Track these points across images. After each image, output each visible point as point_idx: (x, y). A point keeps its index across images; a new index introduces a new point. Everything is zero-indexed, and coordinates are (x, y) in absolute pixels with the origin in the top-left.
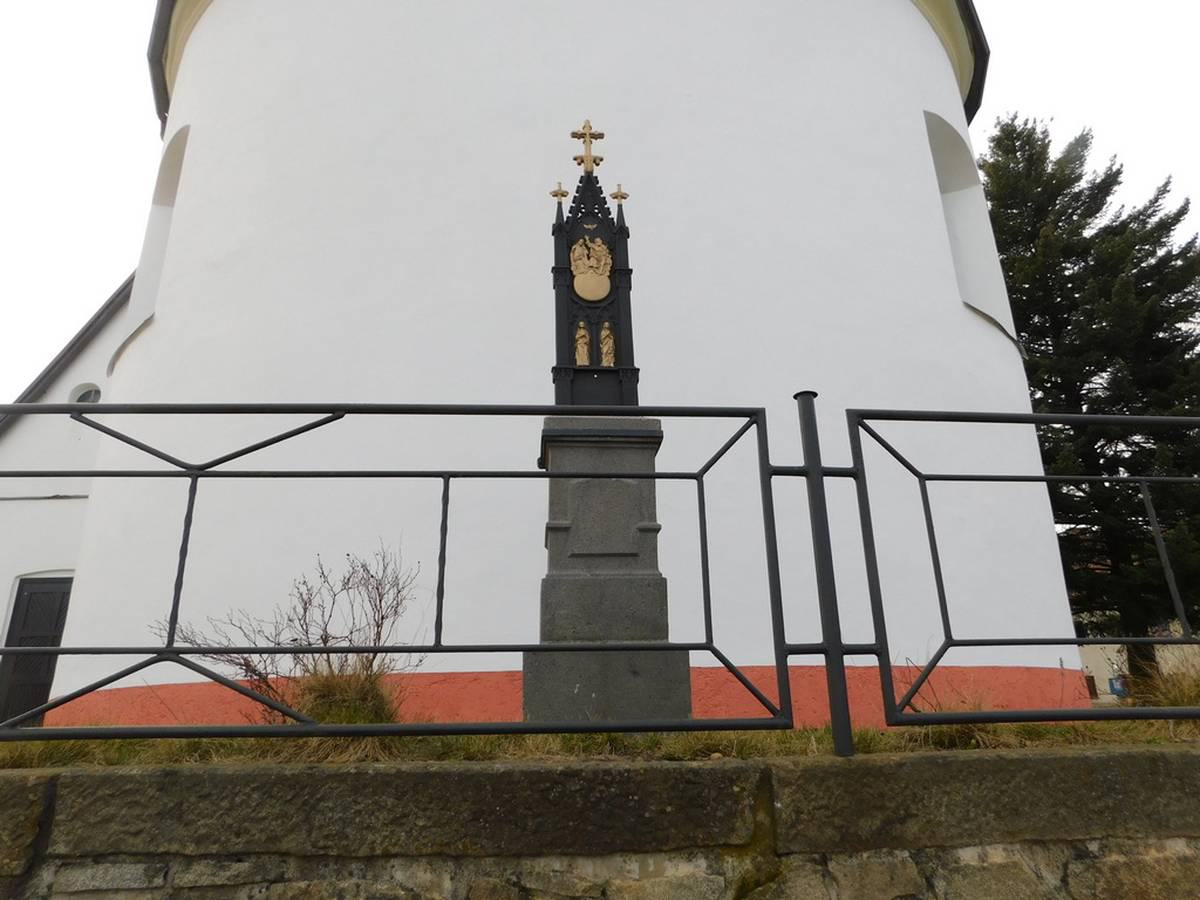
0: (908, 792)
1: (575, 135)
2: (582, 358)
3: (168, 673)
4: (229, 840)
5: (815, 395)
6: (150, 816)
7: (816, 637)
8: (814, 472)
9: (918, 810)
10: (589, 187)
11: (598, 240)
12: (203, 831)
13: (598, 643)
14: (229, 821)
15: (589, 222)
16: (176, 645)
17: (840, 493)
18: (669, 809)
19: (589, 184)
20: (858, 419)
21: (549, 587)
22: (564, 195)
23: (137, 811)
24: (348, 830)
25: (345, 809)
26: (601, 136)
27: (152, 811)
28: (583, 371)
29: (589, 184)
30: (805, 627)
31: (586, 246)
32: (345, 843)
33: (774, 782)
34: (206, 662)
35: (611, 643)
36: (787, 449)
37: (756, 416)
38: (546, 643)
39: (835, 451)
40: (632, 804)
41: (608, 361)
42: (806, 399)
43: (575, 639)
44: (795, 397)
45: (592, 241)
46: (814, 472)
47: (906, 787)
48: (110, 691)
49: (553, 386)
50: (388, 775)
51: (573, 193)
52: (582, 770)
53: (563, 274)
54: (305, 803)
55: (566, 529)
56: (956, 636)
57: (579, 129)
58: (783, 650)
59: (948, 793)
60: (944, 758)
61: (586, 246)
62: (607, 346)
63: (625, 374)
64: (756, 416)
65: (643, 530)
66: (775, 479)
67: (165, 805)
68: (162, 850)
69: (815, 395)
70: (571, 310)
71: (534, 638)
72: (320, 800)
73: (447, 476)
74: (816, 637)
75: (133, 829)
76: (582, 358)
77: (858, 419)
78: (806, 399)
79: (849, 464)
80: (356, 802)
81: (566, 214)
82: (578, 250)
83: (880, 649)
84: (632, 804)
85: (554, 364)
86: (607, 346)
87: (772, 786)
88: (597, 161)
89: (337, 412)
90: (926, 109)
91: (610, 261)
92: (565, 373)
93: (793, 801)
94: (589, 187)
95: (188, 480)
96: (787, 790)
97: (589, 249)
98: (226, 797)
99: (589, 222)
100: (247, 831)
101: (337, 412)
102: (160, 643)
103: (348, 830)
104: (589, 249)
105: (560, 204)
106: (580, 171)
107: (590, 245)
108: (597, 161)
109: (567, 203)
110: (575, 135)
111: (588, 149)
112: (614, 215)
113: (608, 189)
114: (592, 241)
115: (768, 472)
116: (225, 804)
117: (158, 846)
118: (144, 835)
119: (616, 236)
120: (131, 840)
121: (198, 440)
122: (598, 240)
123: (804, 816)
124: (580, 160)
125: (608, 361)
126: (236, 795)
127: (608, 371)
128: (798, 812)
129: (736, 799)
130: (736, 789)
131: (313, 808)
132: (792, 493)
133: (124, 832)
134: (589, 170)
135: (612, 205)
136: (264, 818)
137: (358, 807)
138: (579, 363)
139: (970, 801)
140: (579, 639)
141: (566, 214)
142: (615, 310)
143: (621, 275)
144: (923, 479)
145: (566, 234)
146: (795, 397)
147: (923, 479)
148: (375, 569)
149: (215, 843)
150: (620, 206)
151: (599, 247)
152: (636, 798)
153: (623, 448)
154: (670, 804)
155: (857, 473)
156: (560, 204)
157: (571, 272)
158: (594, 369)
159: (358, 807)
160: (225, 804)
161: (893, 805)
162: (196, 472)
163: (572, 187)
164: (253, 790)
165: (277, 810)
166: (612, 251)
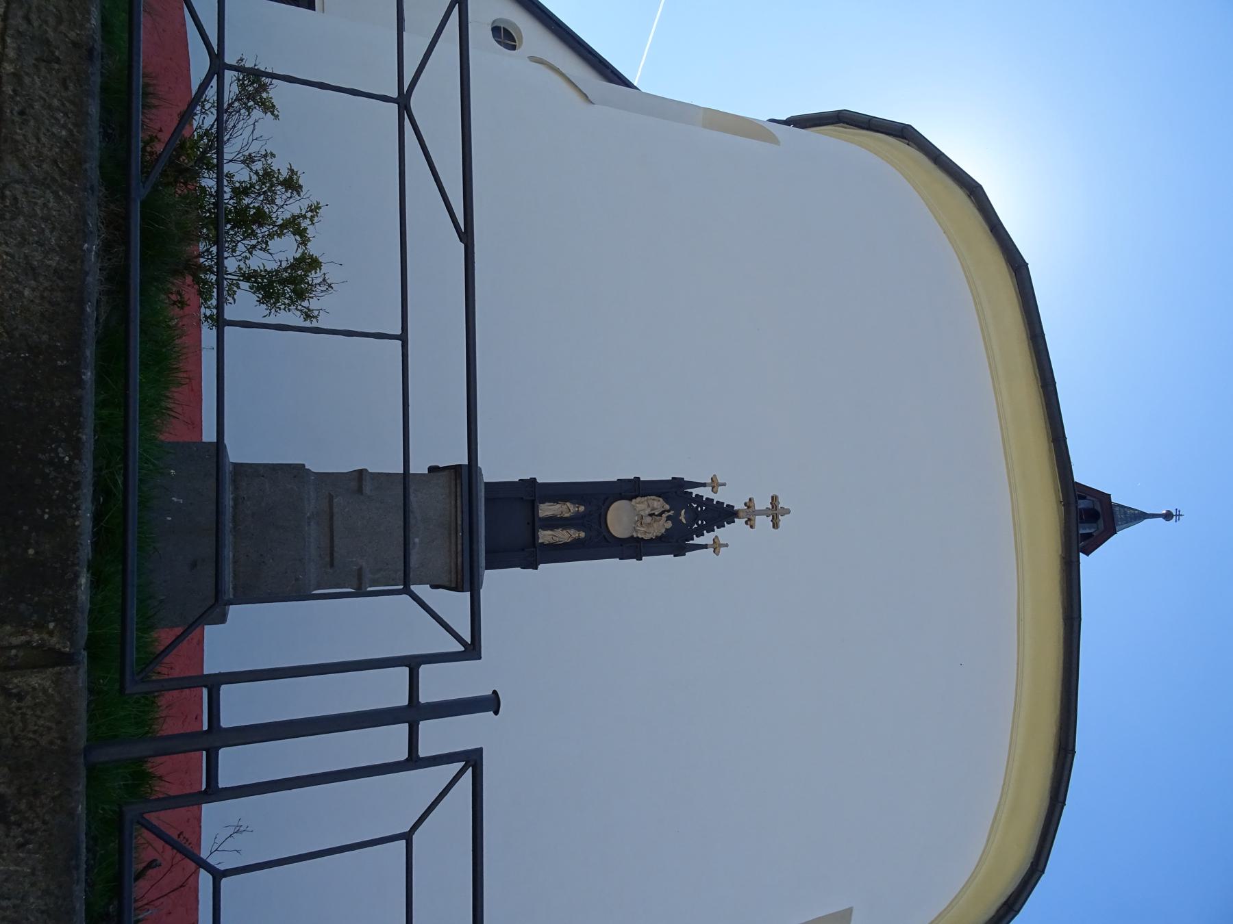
0: (37, 824)
1: (774, 499)
2: (547, 510)
3: (199, 64)
4: (17, 103)
5: (496, 713)
6: (46, 32)
7: (228, 720)
8: (414, 713)
9: (15, 837)
10: (723, 515)
11: (669, 525)
12: (27, 80)
13: (228, 524)
14: (37, 106)
15: (687, 516)
16: (227, 72)
17: (390, 742)
18: (31, 551)
19: (724, 515)
20: (473, 760)
21: (298, 471)
22: (714, 490)
23: (51, 20)
24: (22, 219)
25: (45, 219)
26: (776, 526)
27: (51, 34)
28: (534, 510)
29: (724, 515)
30: (238, 707)
31: (663, 512)
32: (8, 216)
33: (57, 669)
34: (211, 93)
35: (229, 539)
36: (438, 684)
37: (472, 650)
38: (228, 469)
39: (437, 736)
40: (39, 511)
41: (545, 536)
42: (491, 703)
43: (235, 500)
44: (495, 692)
45: (668, 518)
46: (414, 713)
47: (44, 822)
48: (184, 25)
49: (515, 479)
50: (83, 262)
51: (716, 498)
52: (80, 460)
53: (633, 489)
54: (54, 179)
55: (360, 490)
56: (224, 881)
57: (782, 504)
58: (215, 683)
59: (33, 873)
60: (77, 867)
61: (663, 512)
62: (564, 536)
63: (531, 554)
64: (472, 650)
65: (360, 574)
66: (423, 753)
67: (57, 48)
68: (9, 40)
69: (496, 713)
70: (595, 498)
71: (236, 454)
72: (55, 193)
73: (403, 338)
74: (228, 720)
75: (33, 16)
76: (547, 510)
77: (473, 760)
78: (491, 703)
79: (423, 753)
80: (53, 229)
81: (695, 491)
82: (658, 504)
83: (214, 793)
84: (39, 511)
85: (539, 481)
86: (564, 536)
87: (53, 666)
88: (750, 522)
89: (466, 235)
90: (854, 912)
91: (647, 537)
92: (529, 493)
93: (34, 689)
94: (723, 515)
95: (395, 95)
96: (48, 684)
97: (660, 515)
98: (63, 105)
99: (687, 516)
100: (25, 122)
101: (466, 235)
102: (230, 59)
103: (22, 219)
104: (660, 515)
105: (704, 485)
106: (739, 506)
107: (664, 516)
108: (750, 522)
109: (706, 493)
110: (774, 499)
111: (761, 513)
112: (697, 540)
113: (723, 533)
114: (668, 518)
115: (413, 664)
116: (56, 103)
117: (12, 37)
118: (25, 26)
119: (675, 542)
120: (20, 13)
121: (435, 103)
122: (669, 525)
123: (14, 703)
124: (749, 504)
125: (545, 536)
126: (66, 114)
127: (534, 536)
128: (20, 697)
129: (40, 626)
130: (51, 625)
131: (49, 187)
132: (389, 689)
133: (30, 7)
134: (741, 514)
135: (707, 538)
136: (38, 140)
137: (47, 232)
138: (542, 506)
139: (22, 899)
140: (235, 507)
141: (695, 491)
142: (597, 543)
143: (634, 548)
144: (408, 837)
145: (674, 491)
146: (495, 692)
147: (408, 837)
148: (314, 277)
149: (14, 91)
150: (705, 546)
151: (661, 527)
152: (46, 516)
153: (450, 551)
154: (36, 553)
155: (414, 761)
156: (704, 485)
157: (635, 497)
158: (535, 523)
159: (47, 232)
160: (56, 103)
161: (23, 806)
162: (403, 102)
163: (723, 496)
164: (70, 131)
165: (45, 151)
166: (659, 539)
